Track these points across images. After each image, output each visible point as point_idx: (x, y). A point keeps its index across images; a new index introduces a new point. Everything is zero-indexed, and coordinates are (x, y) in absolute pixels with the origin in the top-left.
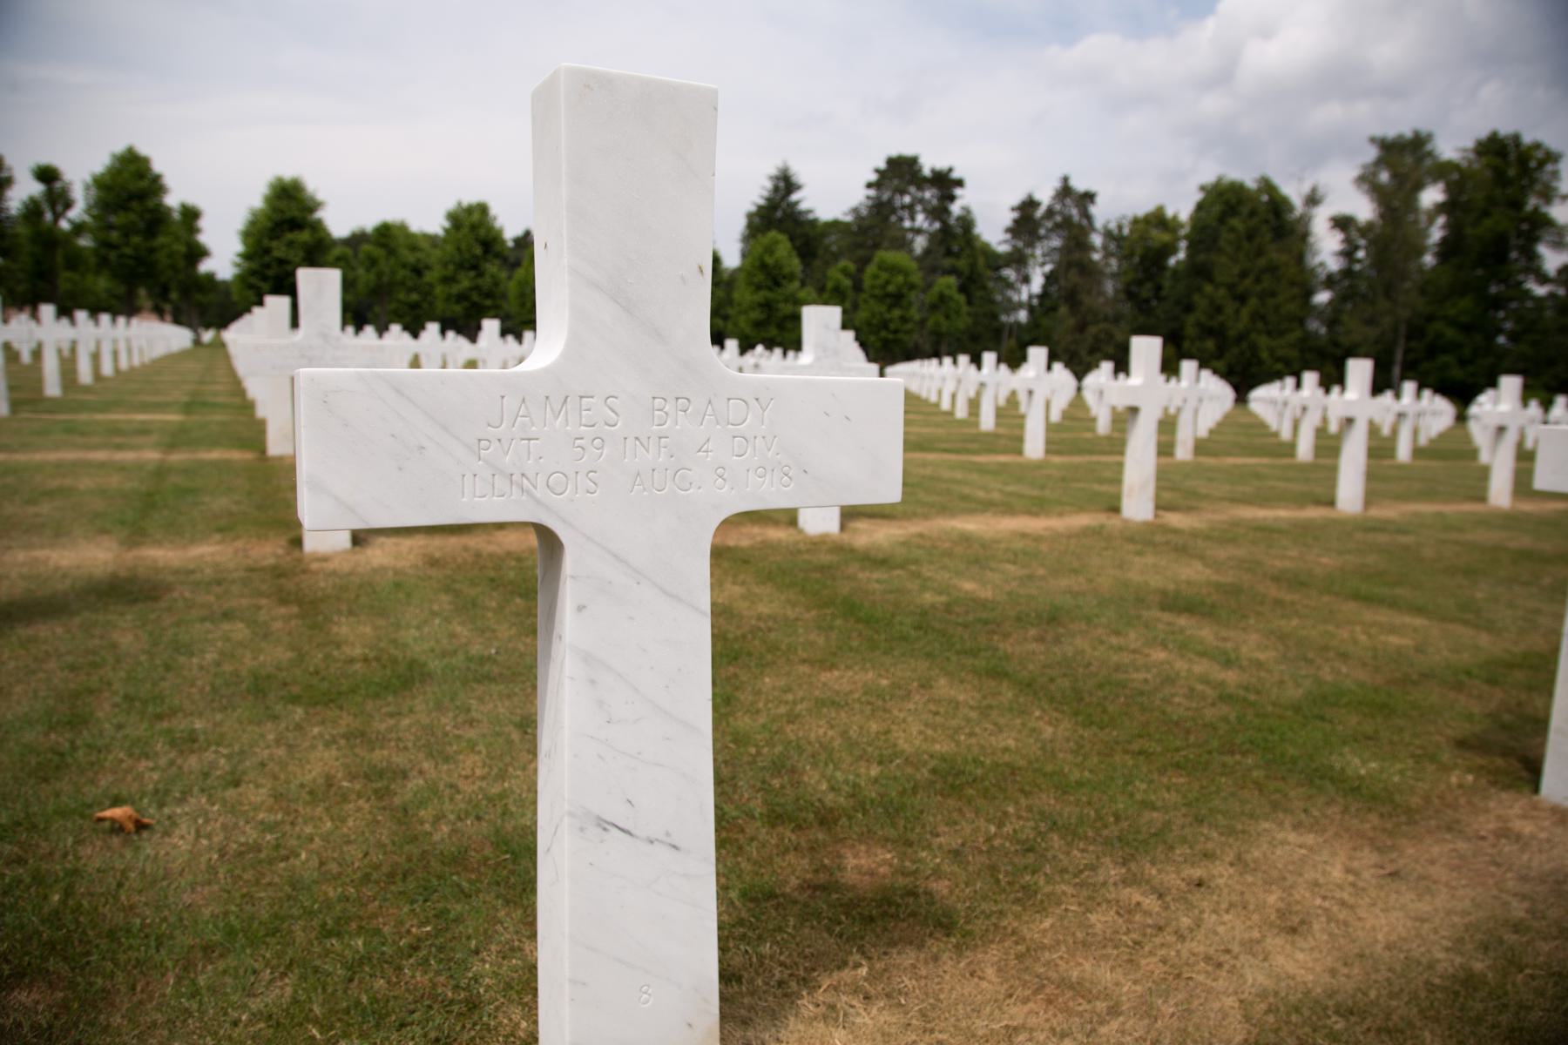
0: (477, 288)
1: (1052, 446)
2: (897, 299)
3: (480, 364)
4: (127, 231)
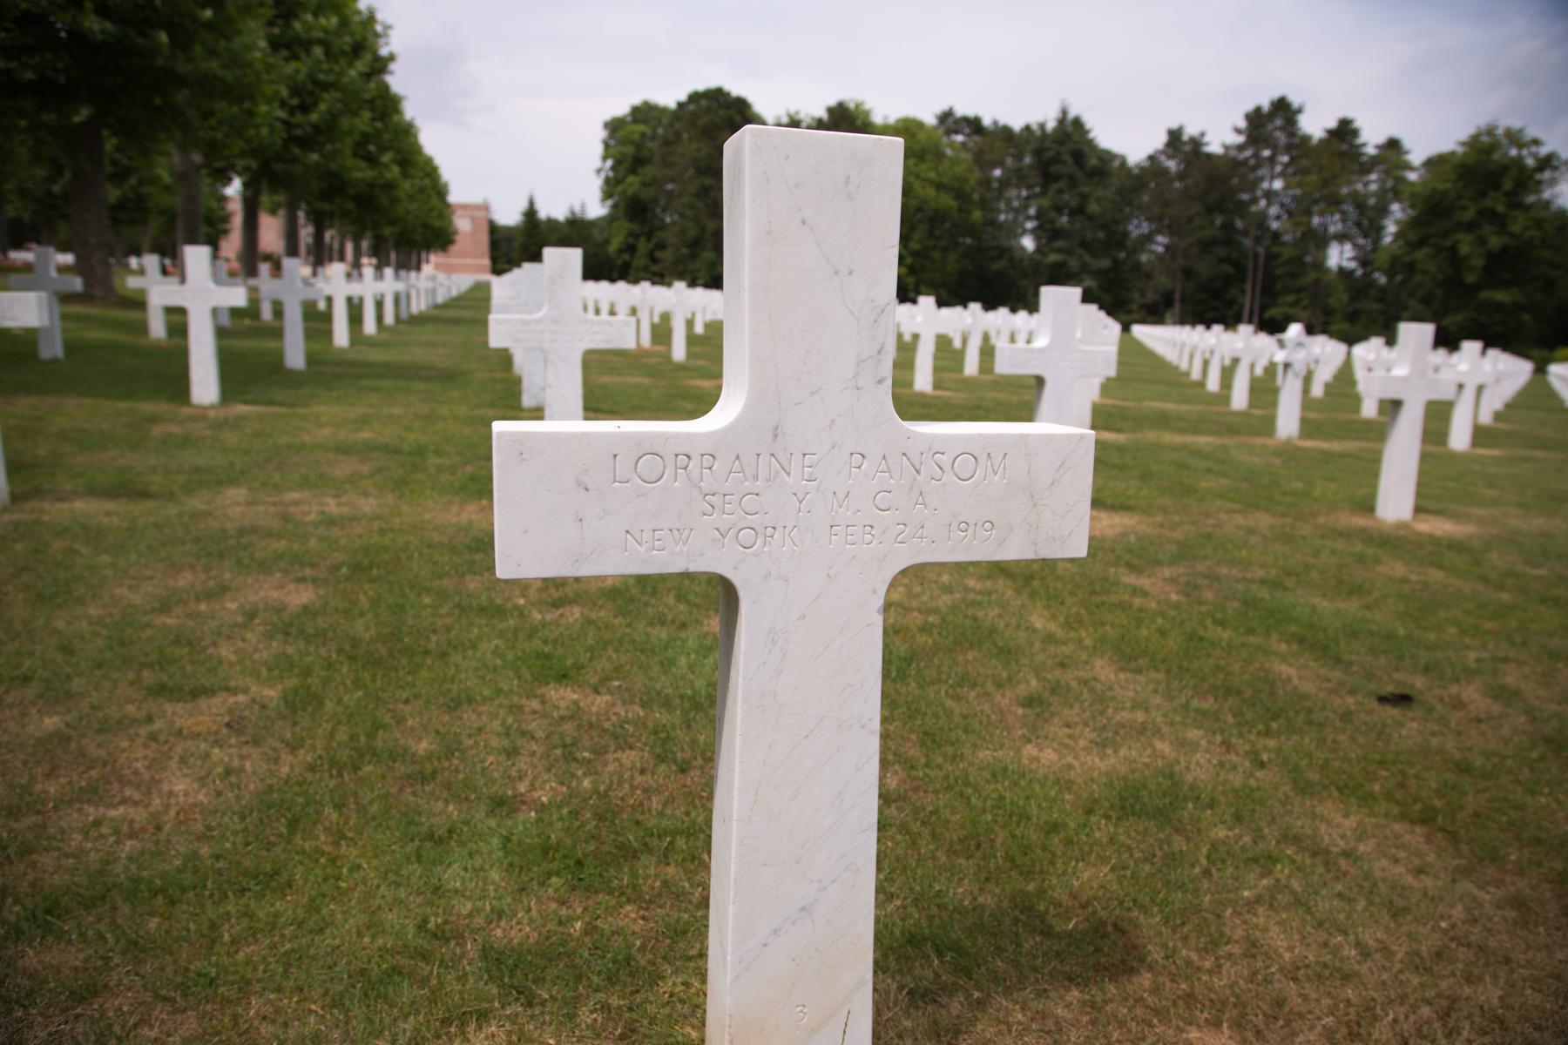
1: (1308, 427)
3: (547, 413)
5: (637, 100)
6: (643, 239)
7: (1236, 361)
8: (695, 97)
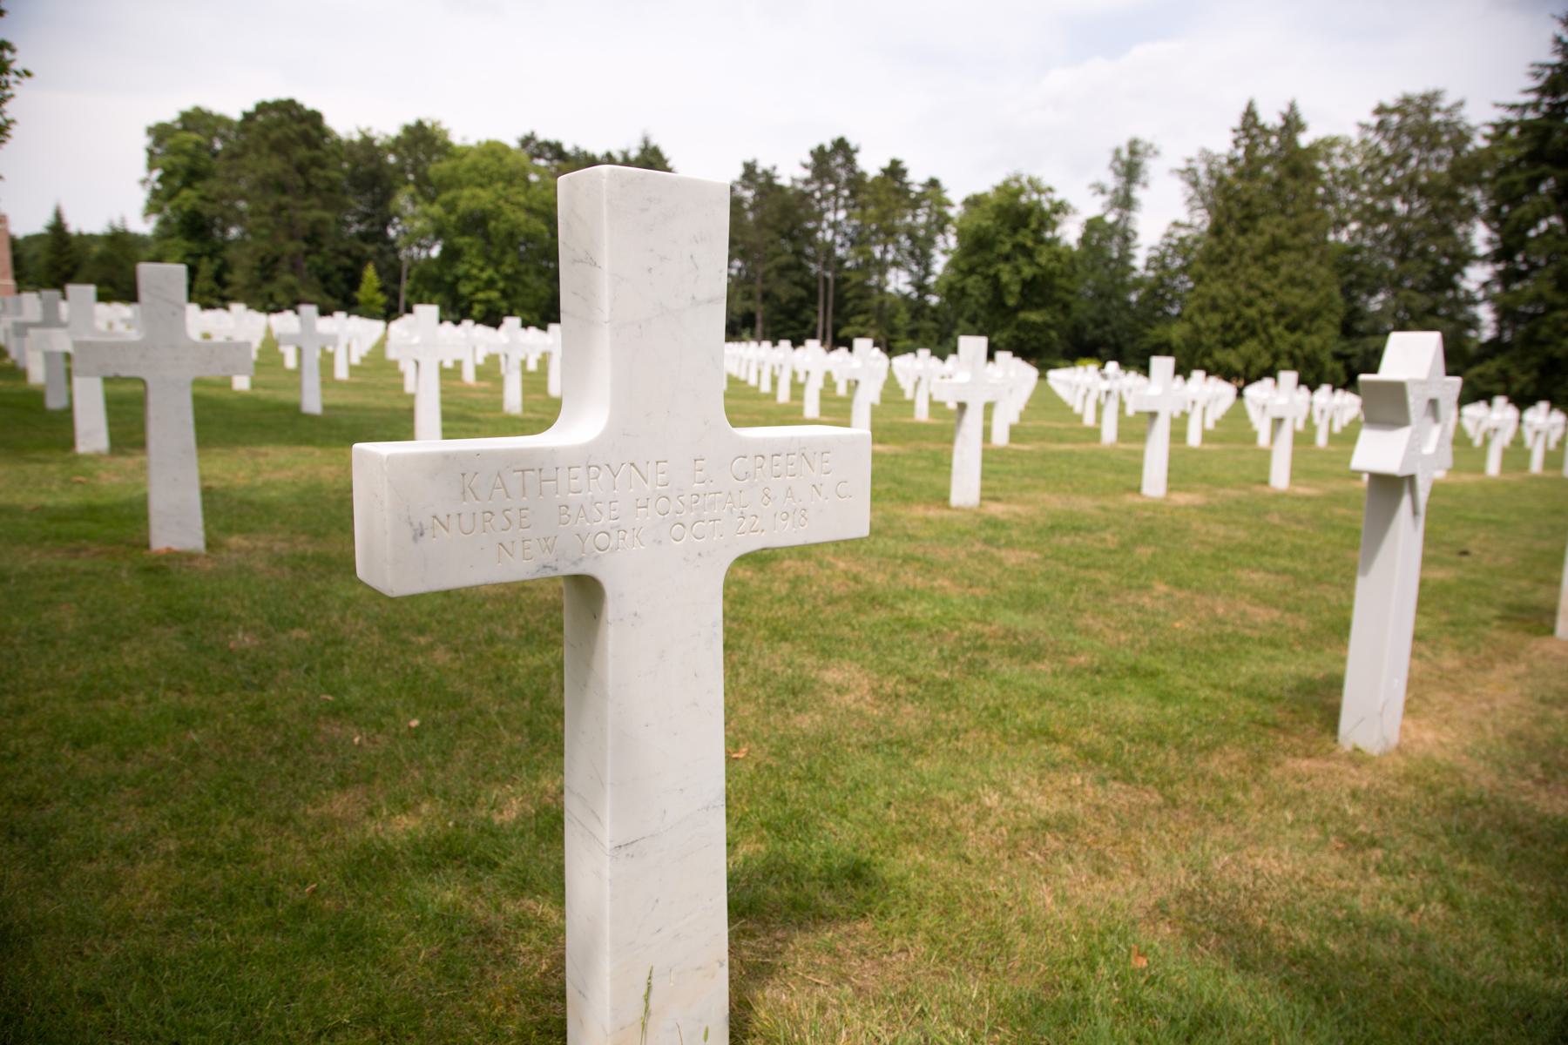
5: (187, 106)
6: (205, 260)
8: (263, 108)
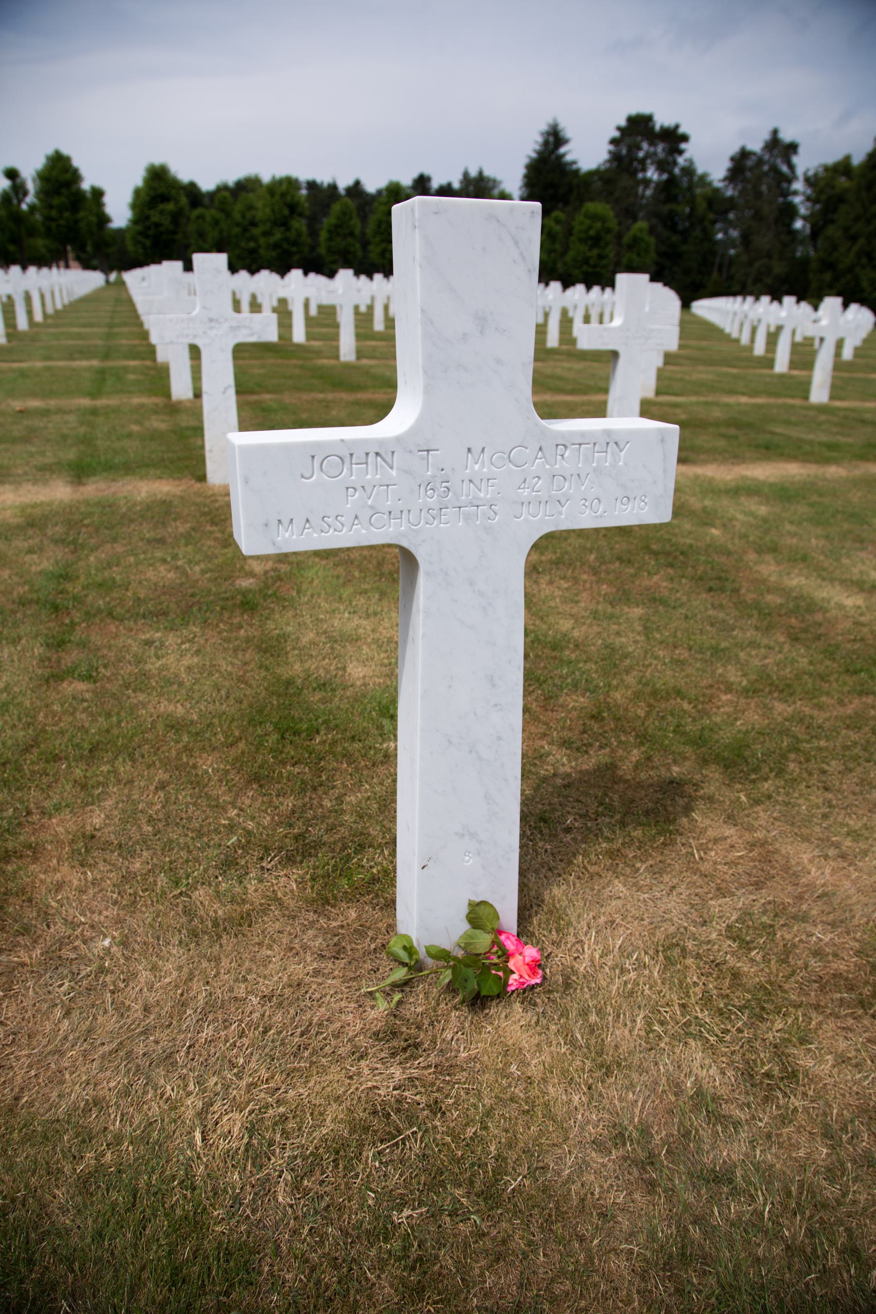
0: (286, 239)
2: (596, 241)
4: (61, 209)
7: (779, 328)
